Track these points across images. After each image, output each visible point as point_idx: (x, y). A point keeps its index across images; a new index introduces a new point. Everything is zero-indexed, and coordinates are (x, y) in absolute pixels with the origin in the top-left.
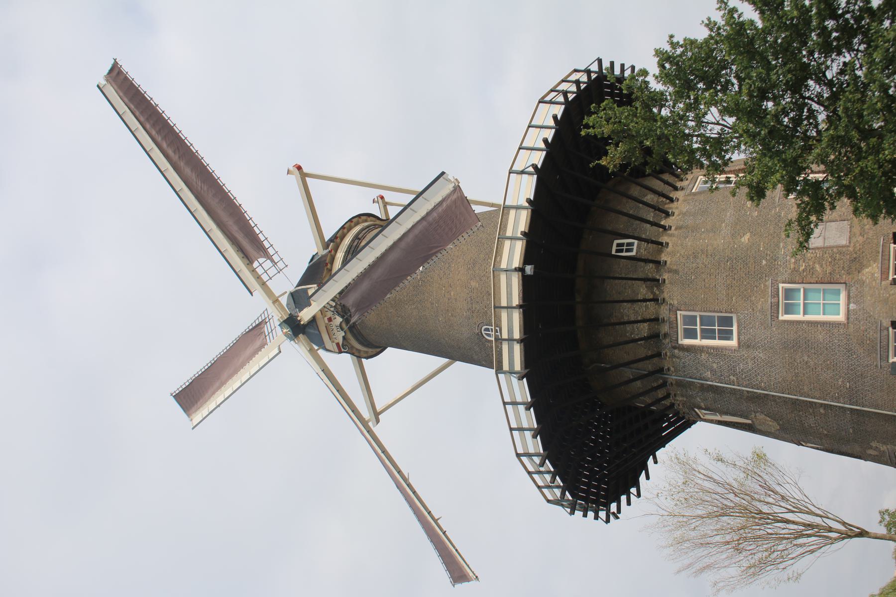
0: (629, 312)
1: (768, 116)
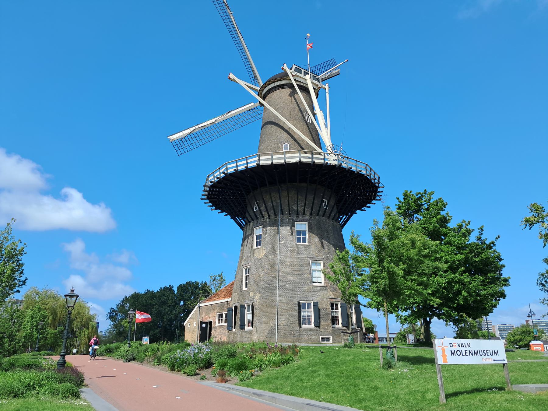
0: (301, 204)
1: (173, 358)
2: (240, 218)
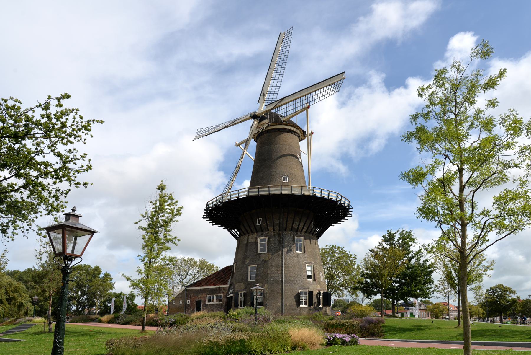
2: (236, 230)
